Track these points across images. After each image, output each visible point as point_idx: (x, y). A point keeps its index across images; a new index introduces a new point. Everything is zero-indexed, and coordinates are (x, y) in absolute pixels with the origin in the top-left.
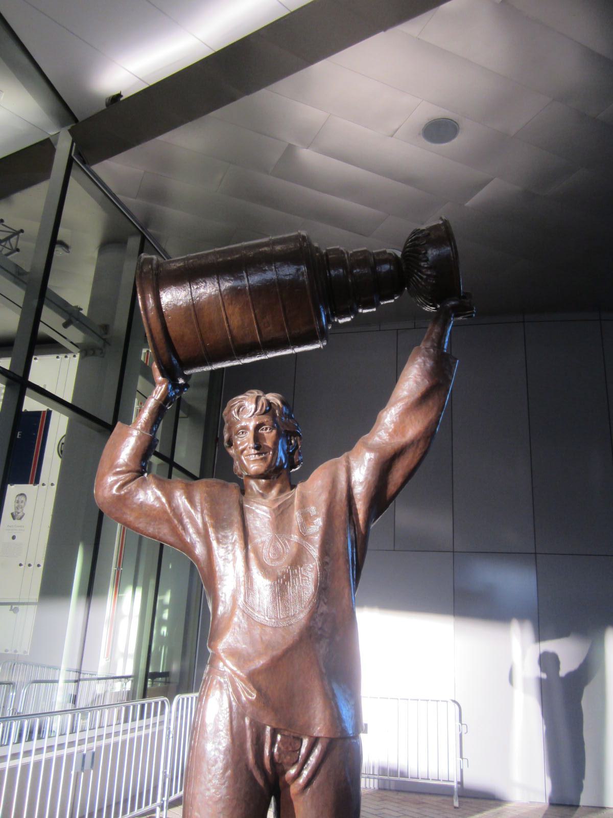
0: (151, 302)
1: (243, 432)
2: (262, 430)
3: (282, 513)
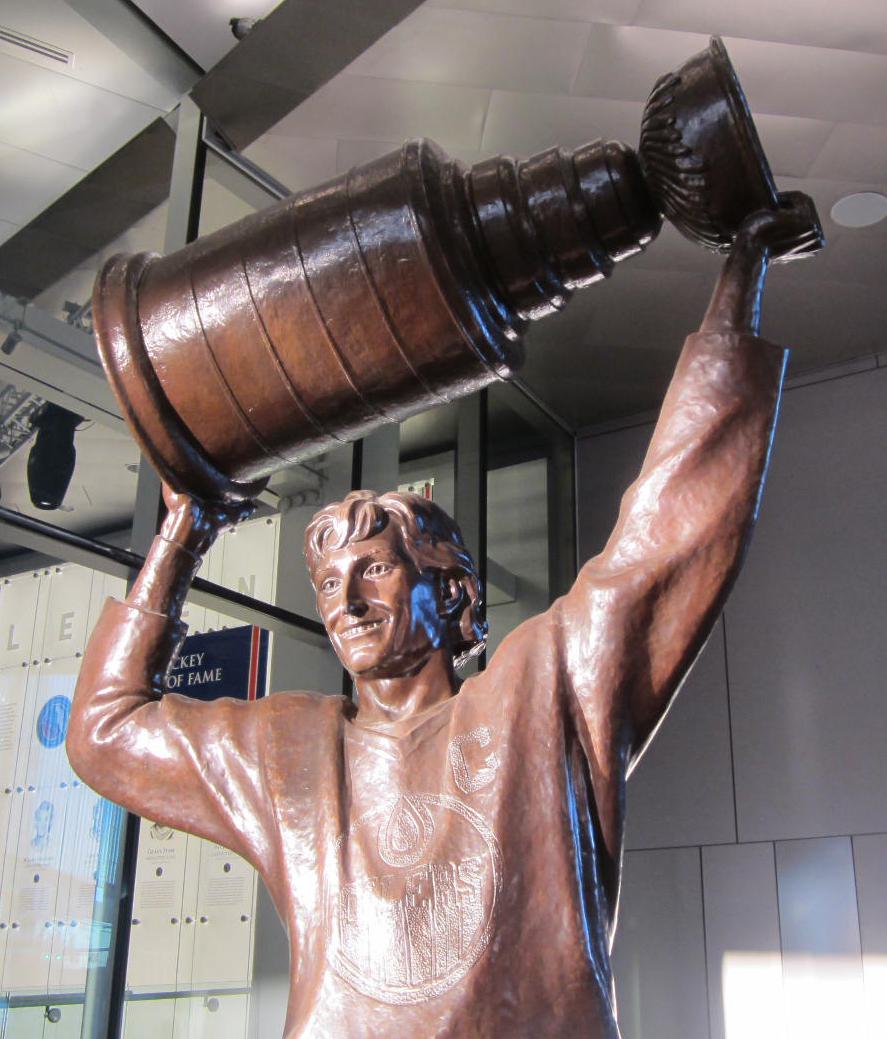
0: (121, 347)
1: (332, 584)
2: (370, 572)
3: (421, 746)
